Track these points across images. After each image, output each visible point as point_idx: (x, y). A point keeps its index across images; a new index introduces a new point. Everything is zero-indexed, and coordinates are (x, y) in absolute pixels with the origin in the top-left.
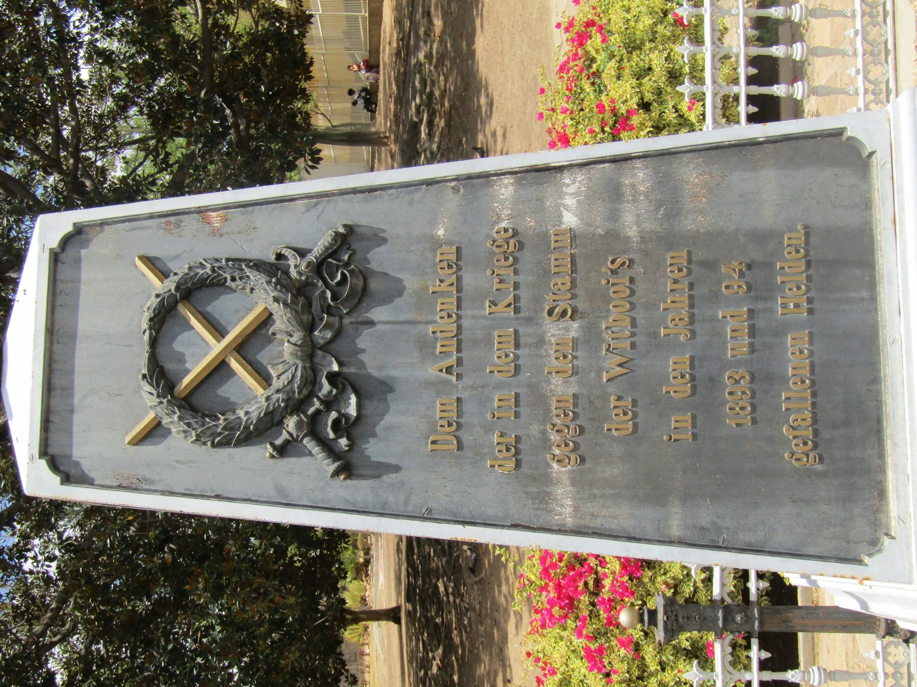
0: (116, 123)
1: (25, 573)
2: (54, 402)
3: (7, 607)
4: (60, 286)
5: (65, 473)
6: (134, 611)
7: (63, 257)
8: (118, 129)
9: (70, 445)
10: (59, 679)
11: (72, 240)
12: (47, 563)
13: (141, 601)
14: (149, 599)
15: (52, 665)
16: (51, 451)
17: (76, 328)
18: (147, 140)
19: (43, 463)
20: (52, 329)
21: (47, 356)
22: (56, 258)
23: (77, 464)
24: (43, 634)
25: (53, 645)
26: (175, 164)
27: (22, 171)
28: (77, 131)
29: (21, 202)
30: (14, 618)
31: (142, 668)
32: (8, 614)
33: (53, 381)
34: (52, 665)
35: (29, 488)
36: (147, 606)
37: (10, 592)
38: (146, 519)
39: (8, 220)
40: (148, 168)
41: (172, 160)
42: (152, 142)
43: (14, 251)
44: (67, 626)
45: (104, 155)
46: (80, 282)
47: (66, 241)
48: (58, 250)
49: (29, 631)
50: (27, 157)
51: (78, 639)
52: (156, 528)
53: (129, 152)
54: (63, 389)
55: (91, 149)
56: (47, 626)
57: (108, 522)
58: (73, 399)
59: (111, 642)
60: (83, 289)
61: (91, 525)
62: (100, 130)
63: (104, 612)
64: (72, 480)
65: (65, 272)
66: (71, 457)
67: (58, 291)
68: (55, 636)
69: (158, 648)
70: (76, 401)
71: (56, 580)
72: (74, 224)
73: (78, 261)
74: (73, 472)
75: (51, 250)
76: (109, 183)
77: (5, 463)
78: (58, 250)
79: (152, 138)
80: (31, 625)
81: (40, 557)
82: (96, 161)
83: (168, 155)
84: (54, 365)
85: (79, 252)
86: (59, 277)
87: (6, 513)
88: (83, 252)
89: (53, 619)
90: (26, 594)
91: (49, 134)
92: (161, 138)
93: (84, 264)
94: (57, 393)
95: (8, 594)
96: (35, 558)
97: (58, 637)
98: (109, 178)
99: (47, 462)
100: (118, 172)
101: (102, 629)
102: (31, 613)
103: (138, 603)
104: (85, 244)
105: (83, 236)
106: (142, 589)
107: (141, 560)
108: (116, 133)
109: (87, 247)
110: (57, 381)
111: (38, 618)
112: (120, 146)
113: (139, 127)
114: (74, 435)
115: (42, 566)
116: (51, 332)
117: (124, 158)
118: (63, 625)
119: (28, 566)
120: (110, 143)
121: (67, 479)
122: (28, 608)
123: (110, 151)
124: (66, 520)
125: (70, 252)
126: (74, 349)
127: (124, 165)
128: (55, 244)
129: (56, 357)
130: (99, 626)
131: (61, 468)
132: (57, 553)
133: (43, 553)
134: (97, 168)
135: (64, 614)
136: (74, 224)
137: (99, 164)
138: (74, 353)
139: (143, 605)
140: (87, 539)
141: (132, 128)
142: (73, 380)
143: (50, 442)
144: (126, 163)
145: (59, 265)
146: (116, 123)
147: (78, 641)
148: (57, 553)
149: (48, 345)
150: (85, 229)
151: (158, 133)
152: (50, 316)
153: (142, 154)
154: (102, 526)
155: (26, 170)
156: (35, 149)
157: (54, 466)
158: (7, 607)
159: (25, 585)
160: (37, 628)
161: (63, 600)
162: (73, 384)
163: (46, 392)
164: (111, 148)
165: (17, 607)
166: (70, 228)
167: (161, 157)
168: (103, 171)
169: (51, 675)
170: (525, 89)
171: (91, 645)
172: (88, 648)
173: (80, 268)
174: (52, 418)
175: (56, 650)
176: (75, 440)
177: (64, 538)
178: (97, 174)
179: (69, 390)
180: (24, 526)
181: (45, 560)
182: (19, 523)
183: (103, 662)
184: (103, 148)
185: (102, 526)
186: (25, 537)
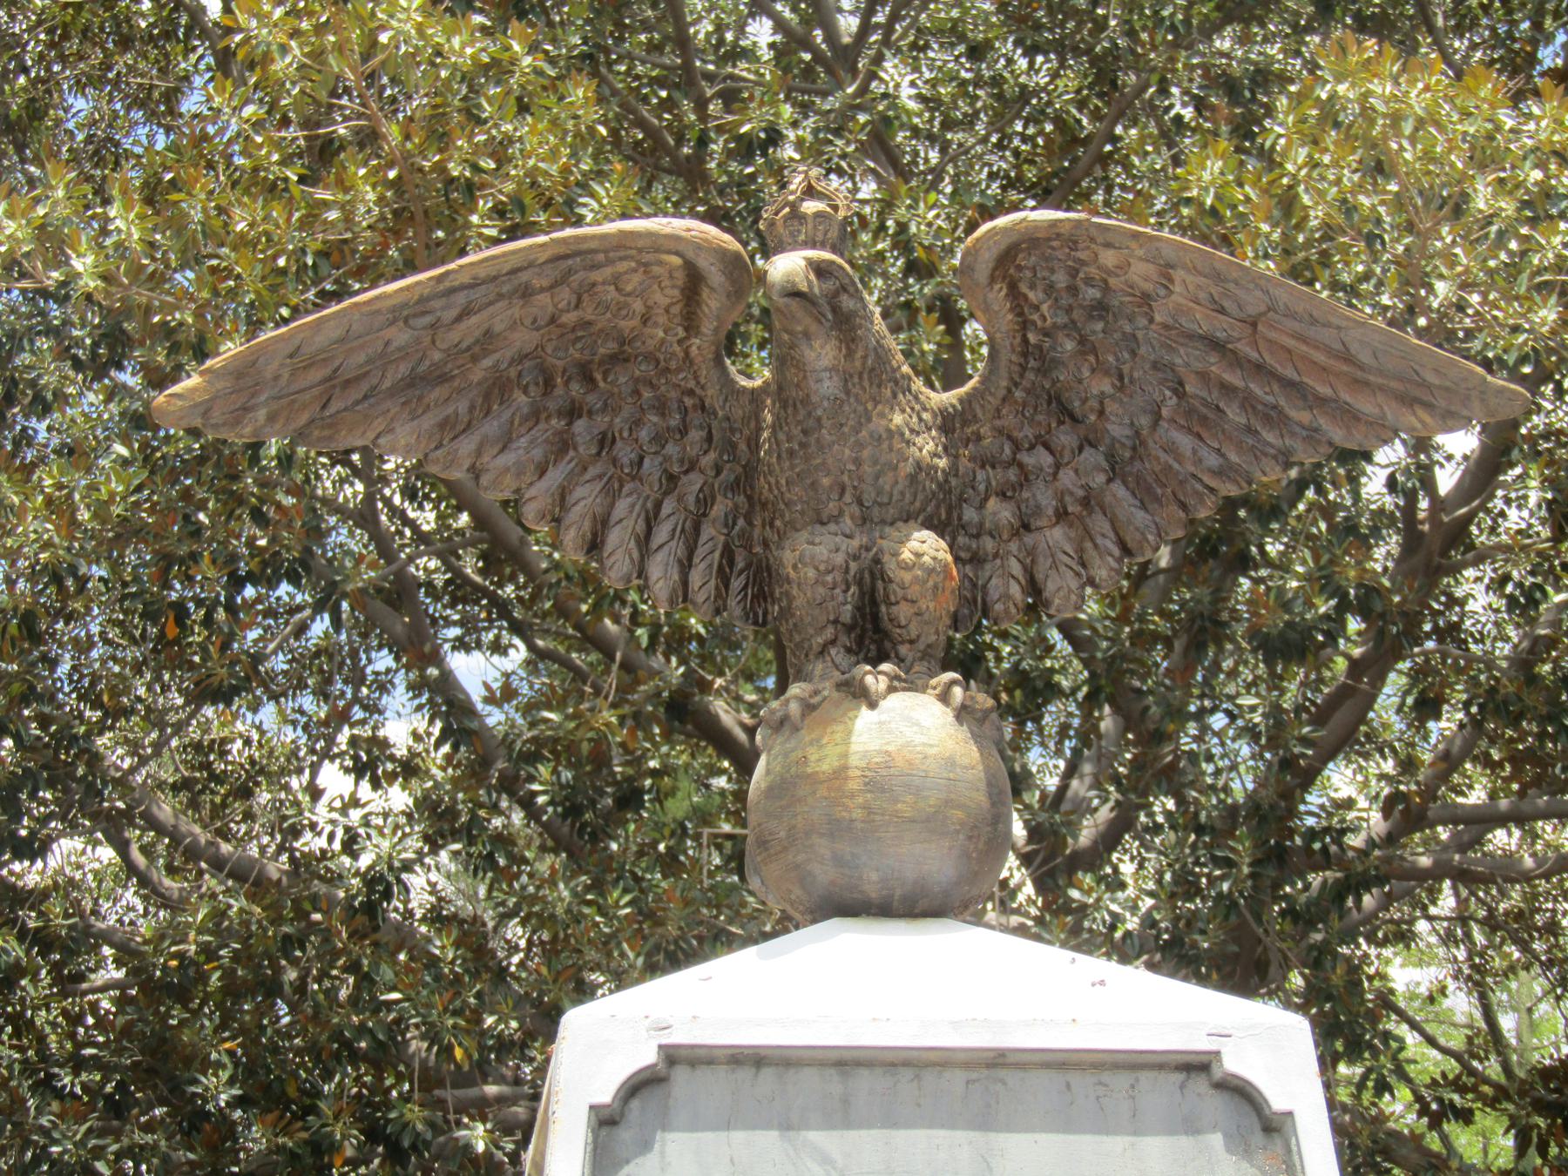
0: (1537, 969)
1: (315, 769)
2: (810, 1076)
3: (223, 725)
4: (1121, 1081)
5: (622, 1114)
6: (206, 1065)
7: (1200, 1084)
8: (1523, 974)
9: (694, 1126)
10: (30, 874)
11: (1247, 1108)
12: (340, 833)
13: (231, 1082)
14: (235, 1103)
15: (66, 847)
16: (680, 1074)
17: (1009, 1127)
18: (1499, 1053)
19: (648, 1056)
20: (1004, 1065)
21: (932, 1056)
22: (1197, 1066)
23: (645, 1146)
24: (152, 823)
25: (122, 847)
26: (1445, 1139)
27: (1386, 726)
28: (1505, 871)
29: (1305, 741)
30: (198, 747)
31: (46, 1087)
32: (206, 731)
33: (865, 1072)
34: (66, 847)
35: (580, 1025)
36: (215, 1098)
37: (262, 733)
38: (455, 1086)
39: (1253, 709)
40: (1427, 1062)
41: (1451, 1127)
42: (1492, 1068)
43: (1171, 727)
44: (167, 882)
45: (1448, 939)
46: (1135, 1133)
47: (1241, 1092)
48: (1217, 1074)
49: (161, 785)
50: (1426, 738)
51: (133, 909)
52: (431, 1124)
53: (1461, 1003)
54: (846, 1102)
55: (1462, 903)
56: (176, 838)
57: (447, 996)
58: (818, 1128)
59: (122, 1002)
60: (1116, 1144)
61: (442, 946)
62: (1518, 926)
63: (203, 978)
64: (604, 1132)
65: (1160, 1091)
66: (665, 1128)
67: (1106, 1077)
68: (143, 849)
69: (102, 1133)
70: (814, 1136)
71: (292, 850)
72: (1290, 1114)
73: (1191, 1126)
74: (625, 1134)
75: (1217, 1053)
76: (1373, 951)
77: (608, 725)
78: (1217, 1074)
79: (1507, 1068)
80: (175, 788)
81: (355, 815)
82: (1430, 918)
83: (1465, 1116)
84: (907, 1073)
85: (1214, 1128)
86: (1145, 1077)
87: (474, 725)
88: (1216, 1140)
89: (193, 853)
90: (257, 771)
91: (1493, 796)
92: (1509, 1098)
93: (1184, 1141)
94: (834, 1084)
95: (259, 728)
96: (355, 802)
97: (140, 859)
98: (1387, 952)
99: (654, 1066)
100: (1404, 975)
101: (158, 987)
102: (205, 787)
103: (225, 1075)
104: (1239, 1144)
105: (1258, 1138)
106: (265, 1092)
107: (346, 1080)
108: (1512, 969)
109: (1229, 1150)
110: (865, 1082)
111: (194, 804)
112: (1478, 979)
113: (1533, 1027)
114: (723, 1135)
115: (333, 822)
116: (995, 1069)
117: (1443, 991)
118: (171, 870)
119: (335, 780)
120: (1482, 955)
121: (605, 1121)
122: (219, 779)
123: (1461, 954)
124: (453, 868)
125: (1215, 1105)
126: (953, 1126)
127: (1423, 990)
128: (1234, 1063)
129: (929, 1077)
130: (165, 967)
131: (635, 1104)
132: (365, 861)
133: (367, 824)
134: (1411, 922)
135: (201, 873)
136: (1290, 1114)
137: (1422, 926)
138: (942, 1126)
139: (218, 1089)
140: (404, 937)
141: (1530, 1010)
142: (870, 1126)
143: (703, 1073)
144: (1431, 999)
145: (1179, 1077)
146: (1537, 969)
147: (125, 908)
148: (365, 861)
149: (962, 1056)
150: (1278, 1141)
151: (1524, 1089)
152: (1037, 1058)
153: (1457, 1042)
154: (438, 978)
155: (1388, 736)
156: (1449, 762)
157: (640, 1085)
158: (223, 725)
159: (283, 771)
160: (165, 809)
161: (244, 875)
162: (860, 1126)
163: (834, 1055)
164: (1470, 958)
165: (223, 754)
166: (1277, 1102)
167: (1456, 1097)
168: (1402, 936)
169: (34, 849)
170: (1548, 389)
171: (112, 945)
172: (106, 937)
173: (1170, 1131)
174: (767, 1073)
175: (107, 853)
176: (709, 1136)
177: (404, 876)
178: (1392, 921)
179: (843, 1116)
180: (439, 775)
181: (347, 829)
182: (448, 758)
183: (68, 982)
184: (1468, 935)
185: (438, 978)
186: (409, 769)
